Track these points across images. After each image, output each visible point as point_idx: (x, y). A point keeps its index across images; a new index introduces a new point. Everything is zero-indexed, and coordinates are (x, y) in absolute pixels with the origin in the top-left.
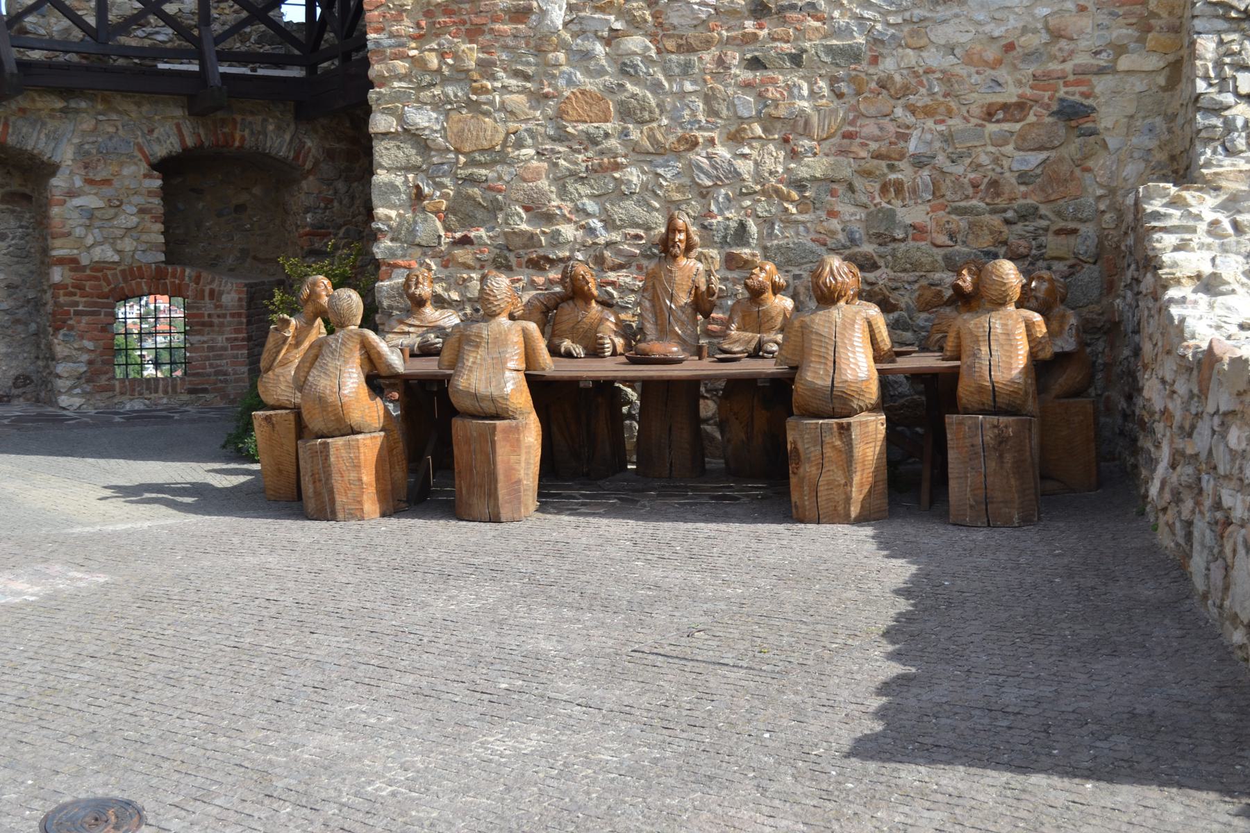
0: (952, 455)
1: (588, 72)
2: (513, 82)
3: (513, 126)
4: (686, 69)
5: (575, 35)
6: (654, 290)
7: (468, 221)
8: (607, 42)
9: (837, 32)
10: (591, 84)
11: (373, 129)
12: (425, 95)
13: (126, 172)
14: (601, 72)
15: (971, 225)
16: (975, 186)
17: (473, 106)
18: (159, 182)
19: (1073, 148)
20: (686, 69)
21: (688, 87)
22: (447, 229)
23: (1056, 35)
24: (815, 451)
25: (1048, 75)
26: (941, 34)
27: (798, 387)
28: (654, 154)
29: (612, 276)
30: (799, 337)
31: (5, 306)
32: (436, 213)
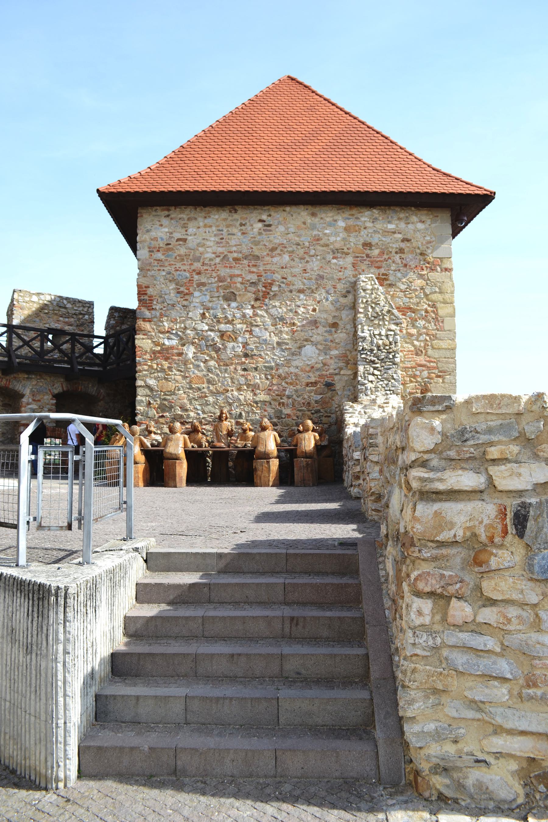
0: (295, 469)
1: (199, 371)
2: (178, 373)
3: (177, 385)
4: (226, 371)
5: (195, 360)
6: (216, 430)
7: (163, 411)
8: (204, 363)
9: (267, 362)
10: (199, 374)
11: (137, 385)
12: (152, 375)
13: (45, 397)
14: (202, 371)
15: (303, 414)
16: (304, 404)
17: (166, 379)
18: (55, 401)
19: (329, 394)
20: (226, 371)
21: (226, 375)
22: (157, 413)
23: (325, 364)
24: (260, 468)
25: (322, 375)
26: (295, 363)
27: (256, 451)
28: (217, 393)
29: (204, 427)
30: (256, 440)
31: (1, 440)
32: (154, 408)
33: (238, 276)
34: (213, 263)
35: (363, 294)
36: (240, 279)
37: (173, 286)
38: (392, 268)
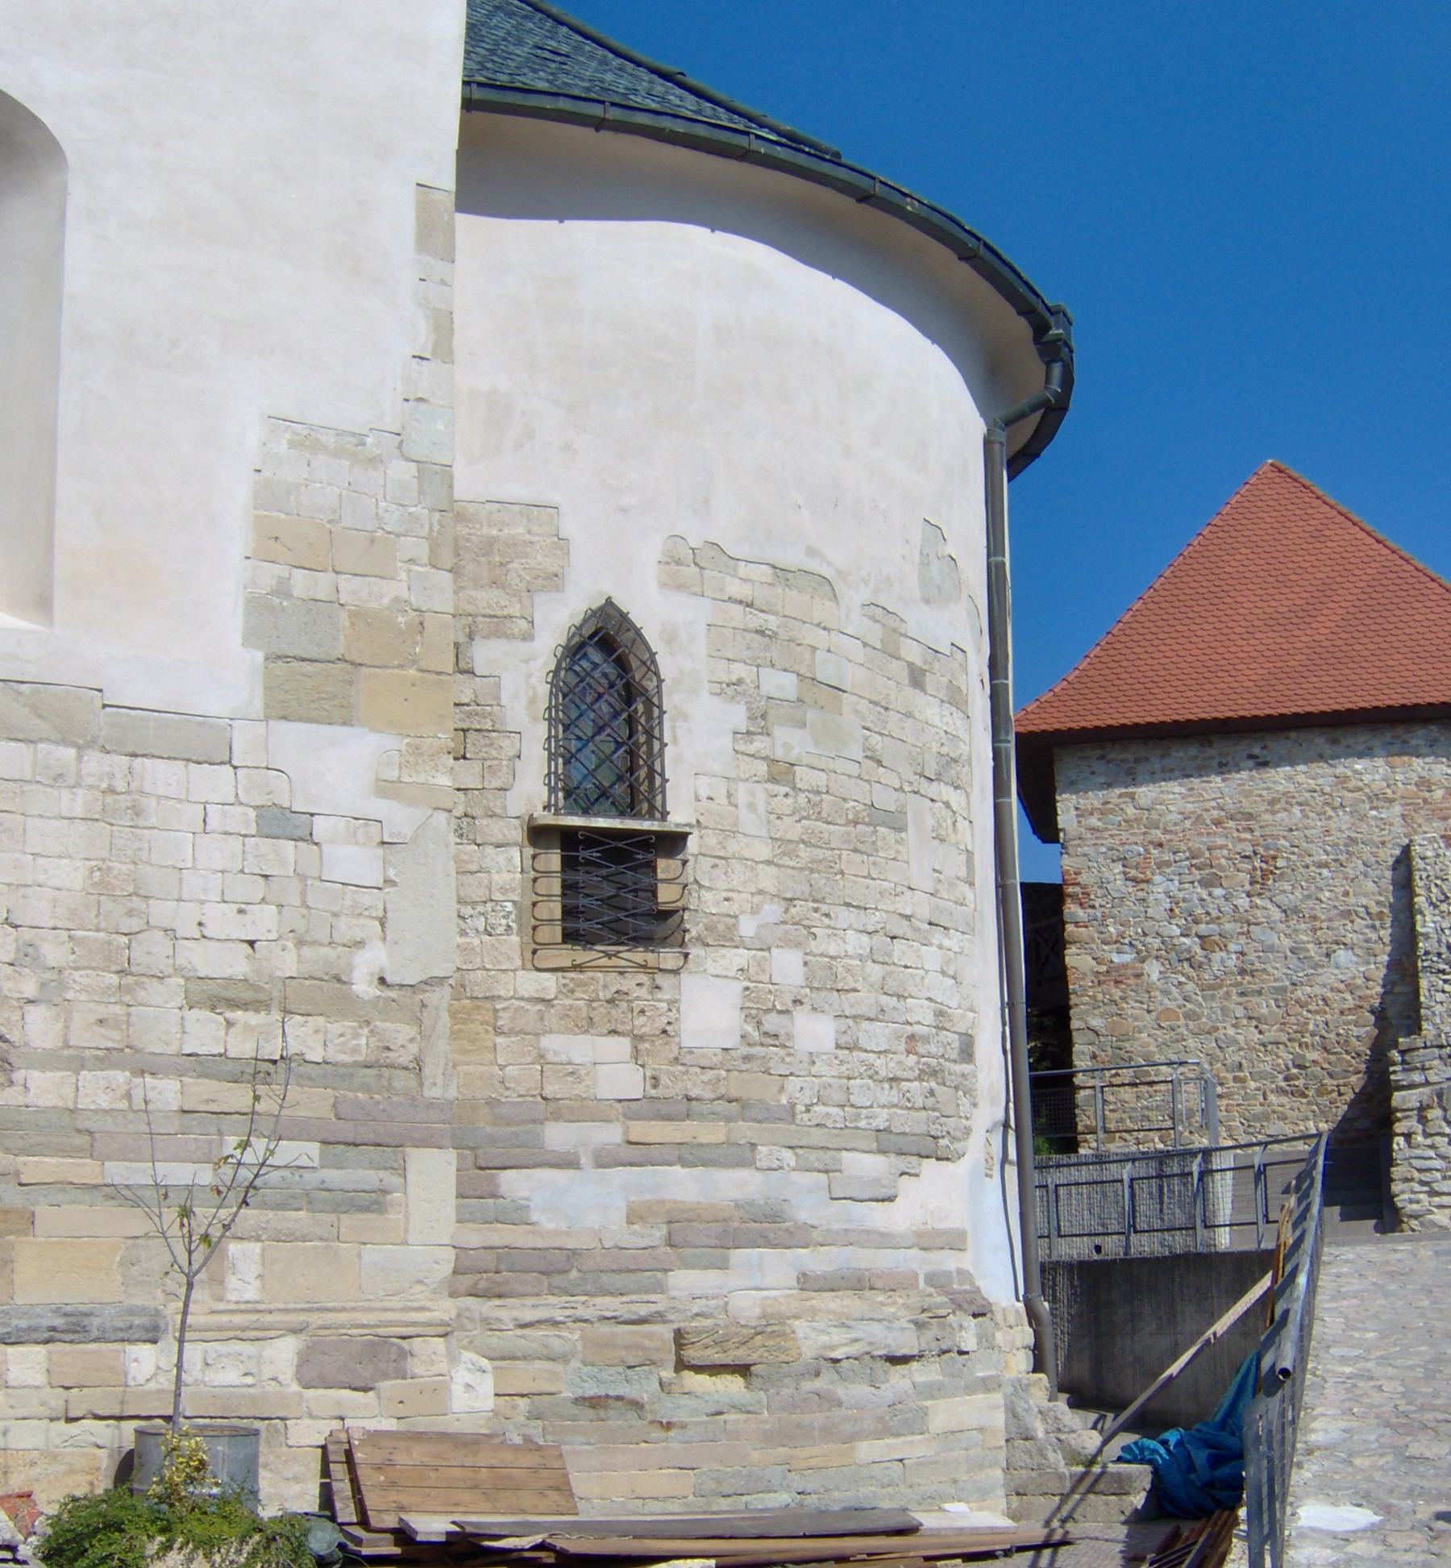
4: (1213, 997)
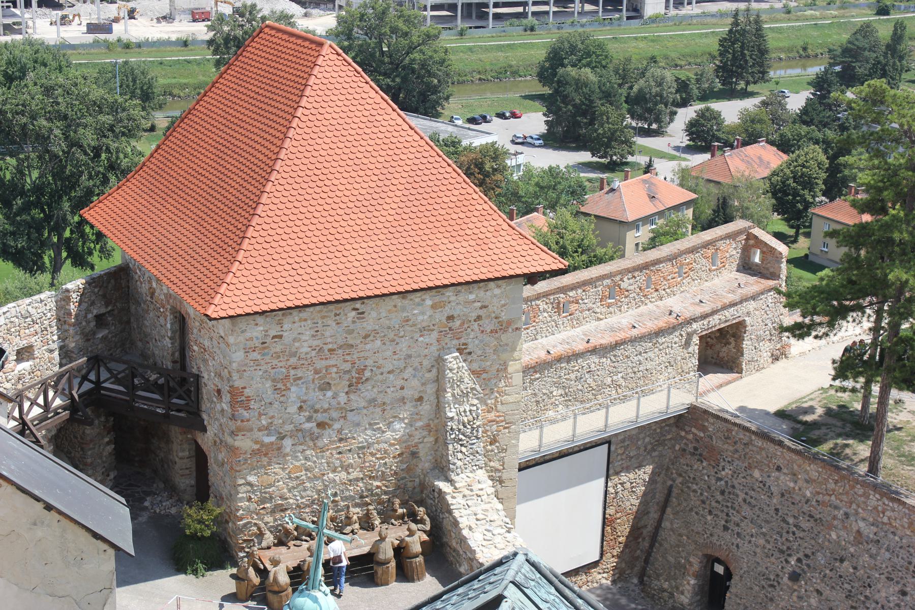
4: (323, 457)
10: (298, 464)
23: (410, 436)
33: (333, 366)
34: (309, 356)
35: (450, 375)
36: (335, 370)
37: (269, 384)
38: (471, 336)
